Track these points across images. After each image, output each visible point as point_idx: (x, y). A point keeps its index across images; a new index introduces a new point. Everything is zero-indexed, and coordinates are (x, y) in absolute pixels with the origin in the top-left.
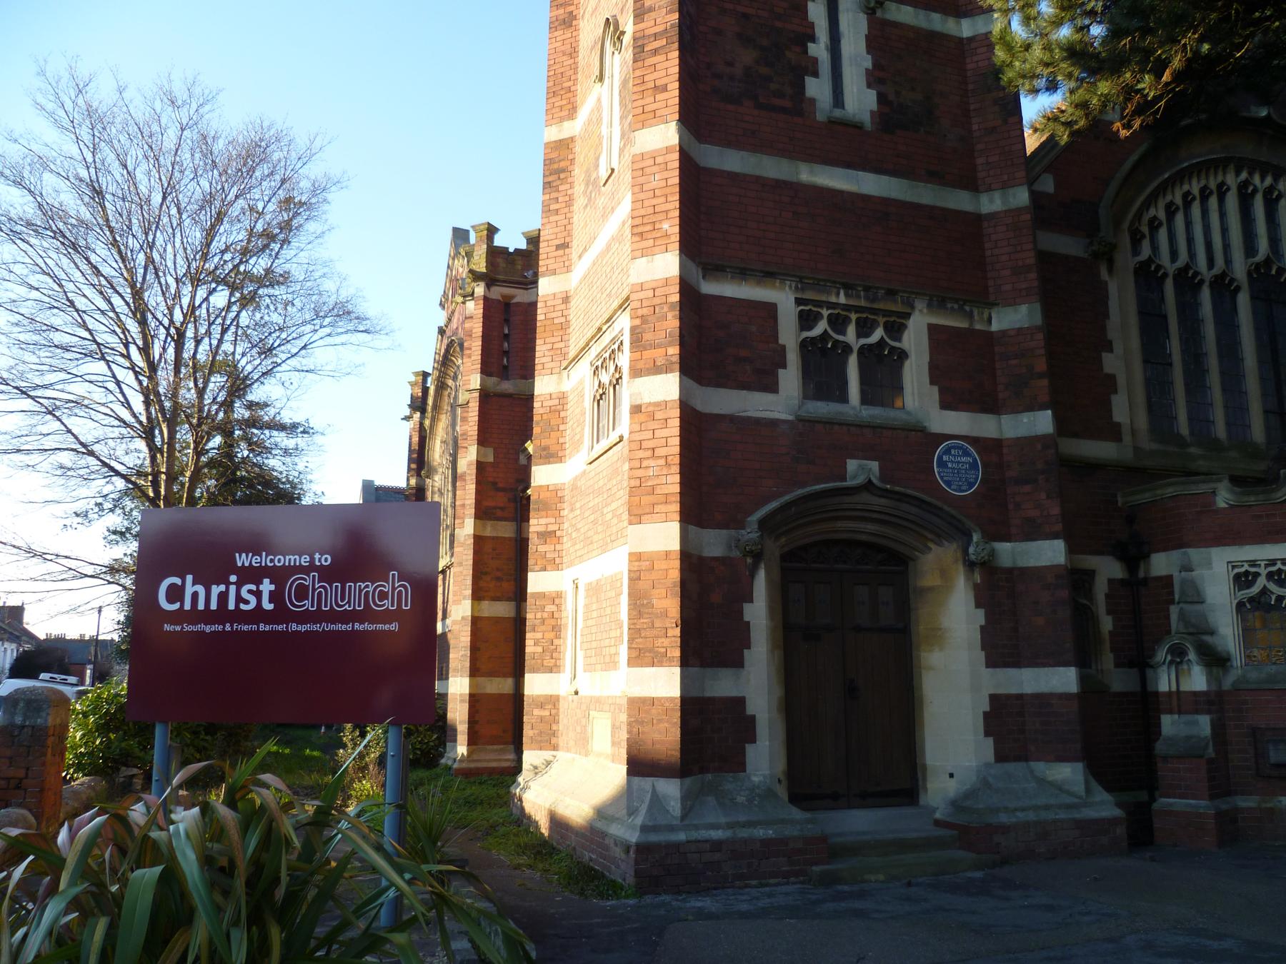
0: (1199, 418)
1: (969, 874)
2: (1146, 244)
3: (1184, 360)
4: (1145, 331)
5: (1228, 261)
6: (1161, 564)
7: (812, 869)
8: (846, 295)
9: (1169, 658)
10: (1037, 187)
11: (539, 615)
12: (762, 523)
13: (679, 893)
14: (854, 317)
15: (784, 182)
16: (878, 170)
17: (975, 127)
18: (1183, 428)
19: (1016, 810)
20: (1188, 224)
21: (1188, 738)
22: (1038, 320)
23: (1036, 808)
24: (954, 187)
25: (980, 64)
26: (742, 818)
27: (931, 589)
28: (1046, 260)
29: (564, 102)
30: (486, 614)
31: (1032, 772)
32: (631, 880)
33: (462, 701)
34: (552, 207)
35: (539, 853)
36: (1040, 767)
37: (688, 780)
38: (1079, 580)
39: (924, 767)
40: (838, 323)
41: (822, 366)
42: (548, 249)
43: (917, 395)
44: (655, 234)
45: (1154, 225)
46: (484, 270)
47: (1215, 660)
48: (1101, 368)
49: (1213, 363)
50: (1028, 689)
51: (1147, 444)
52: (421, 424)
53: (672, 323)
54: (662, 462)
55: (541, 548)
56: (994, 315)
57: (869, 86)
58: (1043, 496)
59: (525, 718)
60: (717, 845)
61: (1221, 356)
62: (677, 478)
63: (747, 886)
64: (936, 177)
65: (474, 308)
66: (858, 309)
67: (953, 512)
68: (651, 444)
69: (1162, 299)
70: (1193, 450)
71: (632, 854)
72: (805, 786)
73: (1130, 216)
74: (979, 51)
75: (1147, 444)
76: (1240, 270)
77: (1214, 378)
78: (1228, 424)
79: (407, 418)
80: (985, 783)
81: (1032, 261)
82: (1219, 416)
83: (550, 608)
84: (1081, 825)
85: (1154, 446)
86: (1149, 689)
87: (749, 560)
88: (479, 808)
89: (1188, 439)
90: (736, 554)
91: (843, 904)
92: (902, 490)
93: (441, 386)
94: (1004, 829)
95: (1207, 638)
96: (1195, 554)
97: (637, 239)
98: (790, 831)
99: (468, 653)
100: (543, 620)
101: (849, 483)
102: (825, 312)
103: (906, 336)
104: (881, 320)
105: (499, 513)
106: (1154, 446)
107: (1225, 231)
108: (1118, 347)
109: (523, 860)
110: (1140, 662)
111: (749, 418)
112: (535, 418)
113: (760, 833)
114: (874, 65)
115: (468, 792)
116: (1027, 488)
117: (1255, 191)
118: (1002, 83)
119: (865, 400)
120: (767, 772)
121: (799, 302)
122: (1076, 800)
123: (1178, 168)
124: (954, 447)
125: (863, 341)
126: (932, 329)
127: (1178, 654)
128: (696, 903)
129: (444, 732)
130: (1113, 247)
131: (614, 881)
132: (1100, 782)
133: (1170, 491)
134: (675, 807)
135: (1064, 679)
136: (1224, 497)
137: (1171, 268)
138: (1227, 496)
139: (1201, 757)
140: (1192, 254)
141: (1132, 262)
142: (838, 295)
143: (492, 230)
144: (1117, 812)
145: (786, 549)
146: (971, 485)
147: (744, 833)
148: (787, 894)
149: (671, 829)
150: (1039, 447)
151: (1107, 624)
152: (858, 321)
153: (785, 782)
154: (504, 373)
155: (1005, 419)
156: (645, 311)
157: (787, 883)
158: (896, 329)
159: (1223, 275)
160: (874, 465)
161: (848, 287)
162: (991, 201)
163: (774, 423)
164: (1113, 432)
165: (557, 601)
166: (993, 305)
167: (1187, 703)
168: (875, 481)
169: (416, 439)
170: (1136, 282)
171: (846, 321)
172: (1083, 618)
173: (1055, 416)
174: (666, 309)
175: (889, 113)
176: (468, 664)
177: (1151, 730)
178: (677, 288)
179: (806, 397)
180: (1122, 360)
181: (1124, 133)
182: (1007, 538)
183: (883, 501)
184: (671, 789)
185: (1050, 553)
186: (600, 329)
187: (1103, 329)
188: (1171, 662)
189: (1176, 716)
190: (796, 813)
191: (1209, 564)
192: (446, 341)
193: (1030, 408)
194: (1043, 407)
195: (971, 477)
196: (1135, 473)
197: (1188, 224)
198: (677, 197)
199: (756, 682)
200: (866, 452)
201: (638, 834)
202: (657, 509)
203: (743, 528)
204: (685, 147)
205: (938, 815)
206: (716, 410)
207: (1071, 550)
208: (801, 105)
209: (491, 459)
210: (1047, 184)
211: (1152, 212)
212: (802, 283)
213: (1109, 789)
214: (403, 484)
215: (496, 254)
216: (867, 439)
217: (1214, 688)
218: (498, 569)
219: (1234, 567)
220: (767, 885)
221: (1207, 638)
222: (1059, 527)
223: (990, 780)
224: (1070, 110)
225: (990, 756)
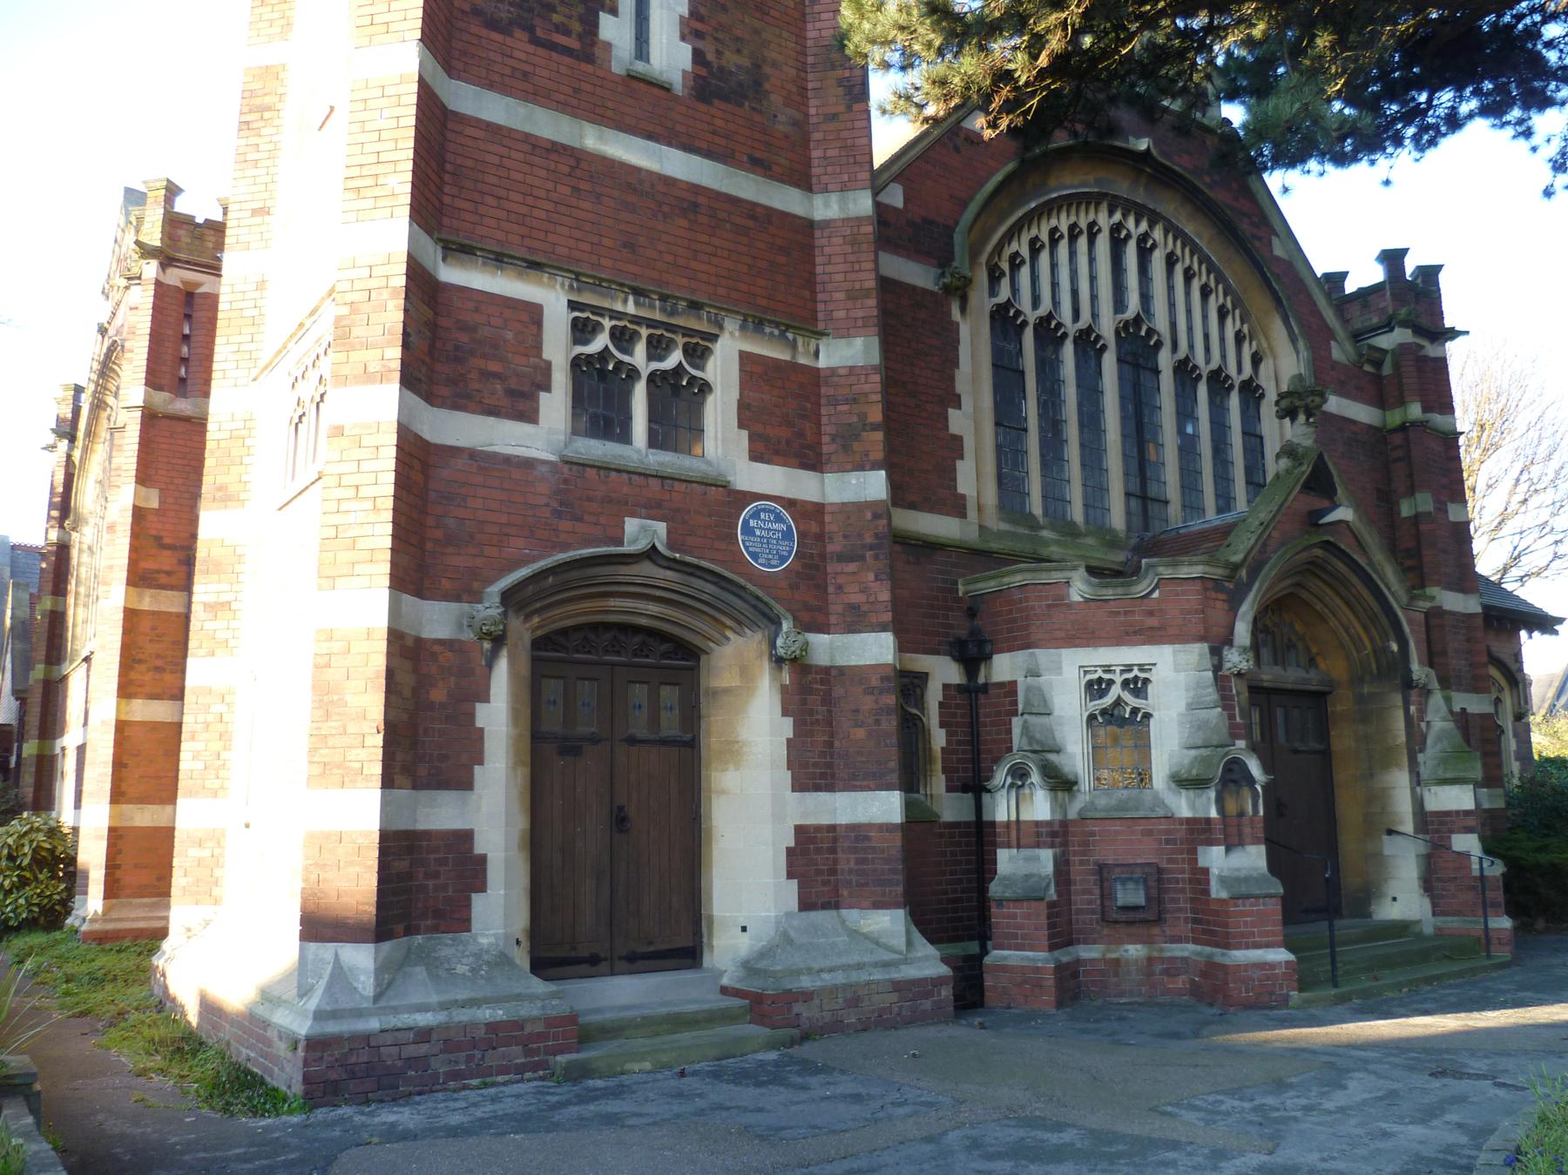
0: (1055, 498)
1: (760, 1056)
2: (1005, 283)
3: (1040, 427)
4: (997, 388)
5: (1095, 316)
6: (1004, 667)
7: (556, 1056)
8: (637, 303)
9: (1009, 780)
10: (881, 198)
11: (201, 718)
12: (506, 596)
13: (367, 1102)
14: (644, 332)
15: (564, 147)
16: (688, 148)
17: (812, 111)
18: (1036, 506)
19: (822, 970)
20: (1054, 266)
21: (1028, 877)
22: (875, 358)
23: (845, 968)
24: (783, 182)
25: (824, 33)
26: (462, 994)
27: (727, 691)
28: (887, 285)
29: (276, 15)
30: (138, 718)
31: (843, 922)
32: (298, 1088)
33: (98, 837)
34: (249, 157)
35: (179, 1049)
36: (852, 916)
37: (387, 946)
38: (910, 684)
39: (711, 919)
40: (623, 338)
41: (599, 397)
42: (240, 214)
43: (721, 442)
44: (377, 192)
46: (158, 243)
47: (1061, 783)
48: (946, 427)
49: (1072, 432)
50: (843, 819)
51: (995, 523)
52: (69, 457)
53: (394, 316)
54: (369, 505)
55: (209, 625)
57: (683, 38)
58: (871, 576)
59: (176, 862)
60: (424, 1035)
61: (1082, 426)
62: (389, 528)
63: (465, 1087)
64: (759, 166)
65: (143, 297)
66: (651, 324)
67: (760, 593)
68: (356, 480)
70: (1045, 533)
71: (301, 1053)
72: (553, 953)
73: (989, 248)
74: (823, 16)
75: (995, 523)
76: (1107, 327)
77: (1073, 452)
78: (1086, 506)
79: (51, 448)
80: (786, 939)
81: (871, 284)
82: (1075, 493)
83: (218, 708)
84: (899, 987)
85: (1004, 526)
86: (986, 818)
87: (487, 645)
88: (109, 987)
89: (1041, 520)
90: (468, 636)
91: (592, 1107)
92: (694, 561)
93: (99, 405)
94: (807, 996)
95: (1052, 757)
96: (1043, 655)
97: (351, 195)
98: (527, 1010)
99: (109, 770)
100: (207, 725)
101: (627, 548)
102: (607, 323)
104: (680, 340)
105: (163, 579)
106: (1004, 526)
107: (1093, 279)
108: (966, 401)
109: (158, 1061)
110: (975, 785)
111: (495, 455)
112: (210, 445)
113: (486, 1014)
114: (692, 13)
115: (98, 963)
117: (1129, 236)
118: (847, 52)
119: (654, 441)
120: (501, 931)
121: (573, 305)
122: (895, 956)
123: (1046, 198)
124: (764, 510)
125: (655, 365)
126: (745, 357)
127: (1020, 773)
128: (388, 1116)
129: (73, 878)
130: (968, 282)
131: (275, 1090)
132: (924, 933)
133: (1018, 579)
134: (366, 984)
135: (884, 807)
136: (1079, 588)
137: (1032, 316)
138: (1083, 587)
139: (1042, 899)
140: (1056, 303)
141: (989, 304)
142: (625, 301)
143: (172, 191)
144: (944, 970)
145: (539, 633)
146: (783, 559)
147: (463, 1016)
148: (518, 1096)
149: (359, 1013)
150: (869, 515)
151: (939, 738)
152: (650, 337)
153: (525, 944)
154: (181, 387)
155: (830, 478)
156: (356, 297)
157: (522, 1080)
158: (698, 353)
159: (1089, 330)
160: (661, 528)
161: (638, 293)
162: (827, 205)
163: (529, 464)
164: (957, 507)
165: (228, 699)
166: (822, 334)
167: (1029, 835)
168: (660, 547)
169: (60, 477)
170: (992, 328)
171: (635, 336)
172: (911, 728)
173: (890, 477)
174: (385, 294)
175: (708, 80)
176: (108, 786)
177: (984, 868)
178: (403, 268)
179: (575, 432)
180: (972, 418)
181: (988, 134)
183: (670, 574)
184: (361, 958)
185: (876, 649)
186: (301, 325)
187: (952, 379)
188: (1012, 785)
189: (1015, 851)
190: (538, 986)
191: (1058, 669)
192: (107, 343)
193: (861, 467)
194: (875, 466)
195: (783, 548)
196: (982, 557)
197: (1054, 266)
198: (411, 144)
199: (490, 810)
200: (652, 509)
201: (309, 1023)
202: (358, 569)
203: (480, 602)
204: (428, 79)
205: (725, 981)
206: (450, 441)
207: (902, 647)
208: (589, 48)
209: (155, 504)
210: (895, 197)
211: (1014, 247)
212: (578, 280)
213: (932, 941)
214: (38, 541)
215: (175, 223)
216: (655, 493)
217: (1058, 817)
218: (158, 656)
219: (1086, 672)
220: (494, 1084)
221: (1052, 757)
222: (888, 617)
223: (792, 933)
224: (927, 87)
225: (793, 903)
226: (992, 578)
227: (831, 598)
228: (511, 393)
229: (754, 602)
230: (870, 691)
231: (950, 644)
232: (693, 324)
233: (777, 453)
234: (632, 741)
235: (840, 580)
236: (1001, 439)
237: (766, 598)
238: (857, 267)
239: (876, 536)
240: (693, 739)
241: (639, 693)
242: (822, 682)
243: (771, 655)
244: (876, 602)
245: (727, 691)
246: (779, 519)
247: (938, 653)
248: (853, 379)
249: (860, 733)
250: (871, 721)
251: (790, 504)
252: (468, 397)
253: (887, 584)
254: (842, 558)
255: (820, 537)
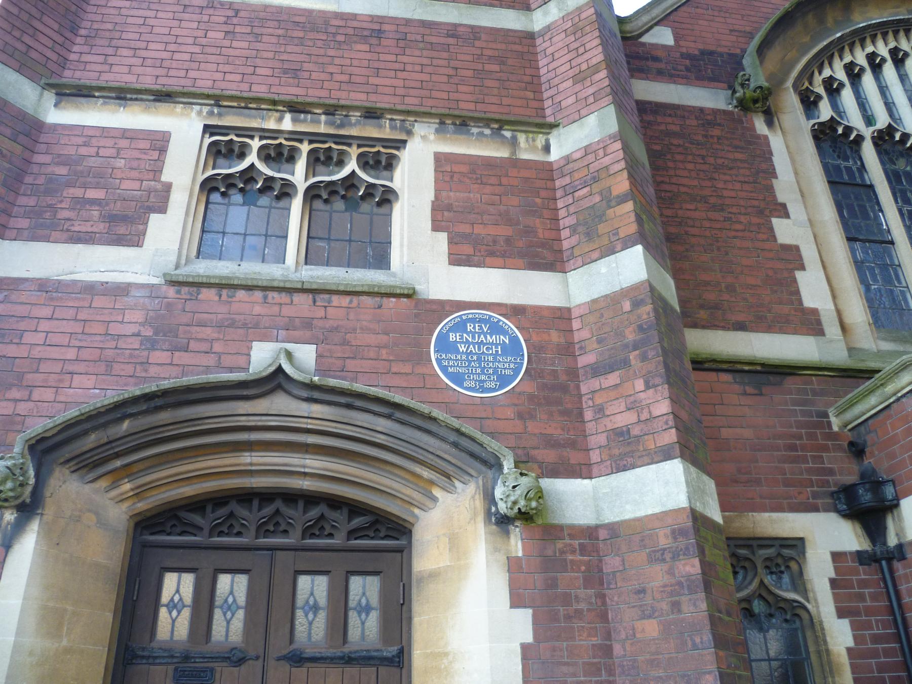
8: (294, 120)
14: (305, 148)
20: (883, 90)
43: (417, 252)
45: (833, 89)
56: (552, 142)
58: (640, 384)
66: (313, 137)
69: (863, 167)
85: (886, 346)
92: (345, 384)
103: (398, 173)
116: (613, 379)
124: (473, 321)
126: (440, 159)
142: (280, 119)
146: (504, 380)
150: (627, 306)
158: (381, 160)
163: (121, 290)
164: (810, 323)
182: (582, 471)
183: (317, 410)
185: (661, 488)
187: (770, 189)
193: (610, 251)
195: (506, 365)
197: (883, 90)
222: (671, 436)
226: (871, 391)
227: (590, 427)
228: (112, 219)
229: (453, 437)
230: (657, 556)
231: (832, 494)
232: (371, 131)
233: (492, 254)
234: (297, 659)
235: (599, 400)
236: (860, 256)
237: (478, 435)
238: (581, 50)
239: (640, 328)
240: (401, 651)
241: (313, 588)
242: (583, 549)
243: (488, 514)
244: (652, 418)
245: (433, 575)
246: (496, 329)
247: (815, 509)
248: (591, 158)
249: (650, 629)
250: (665, 606)
251: (516, 312)
252: (53, 227)
253: (664, 390)
254: (597, 371)
255: (568, 350)
